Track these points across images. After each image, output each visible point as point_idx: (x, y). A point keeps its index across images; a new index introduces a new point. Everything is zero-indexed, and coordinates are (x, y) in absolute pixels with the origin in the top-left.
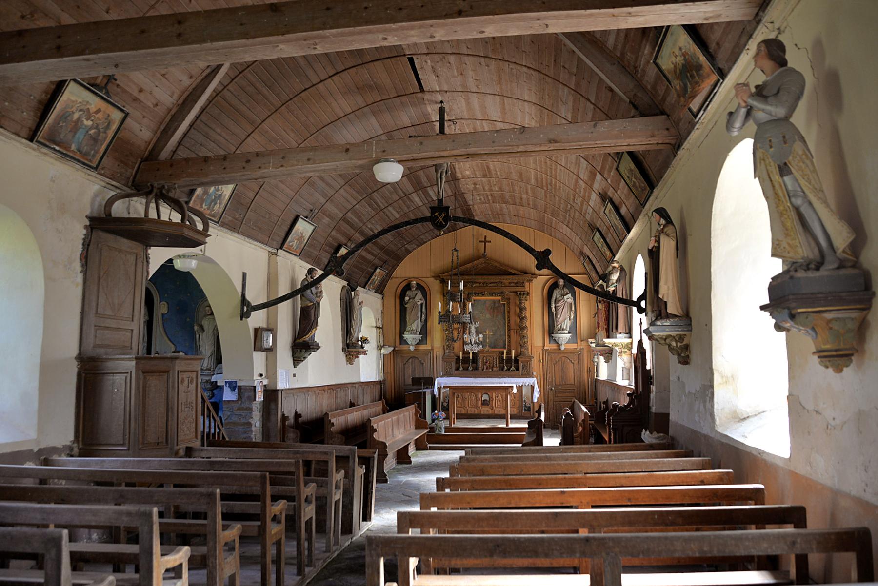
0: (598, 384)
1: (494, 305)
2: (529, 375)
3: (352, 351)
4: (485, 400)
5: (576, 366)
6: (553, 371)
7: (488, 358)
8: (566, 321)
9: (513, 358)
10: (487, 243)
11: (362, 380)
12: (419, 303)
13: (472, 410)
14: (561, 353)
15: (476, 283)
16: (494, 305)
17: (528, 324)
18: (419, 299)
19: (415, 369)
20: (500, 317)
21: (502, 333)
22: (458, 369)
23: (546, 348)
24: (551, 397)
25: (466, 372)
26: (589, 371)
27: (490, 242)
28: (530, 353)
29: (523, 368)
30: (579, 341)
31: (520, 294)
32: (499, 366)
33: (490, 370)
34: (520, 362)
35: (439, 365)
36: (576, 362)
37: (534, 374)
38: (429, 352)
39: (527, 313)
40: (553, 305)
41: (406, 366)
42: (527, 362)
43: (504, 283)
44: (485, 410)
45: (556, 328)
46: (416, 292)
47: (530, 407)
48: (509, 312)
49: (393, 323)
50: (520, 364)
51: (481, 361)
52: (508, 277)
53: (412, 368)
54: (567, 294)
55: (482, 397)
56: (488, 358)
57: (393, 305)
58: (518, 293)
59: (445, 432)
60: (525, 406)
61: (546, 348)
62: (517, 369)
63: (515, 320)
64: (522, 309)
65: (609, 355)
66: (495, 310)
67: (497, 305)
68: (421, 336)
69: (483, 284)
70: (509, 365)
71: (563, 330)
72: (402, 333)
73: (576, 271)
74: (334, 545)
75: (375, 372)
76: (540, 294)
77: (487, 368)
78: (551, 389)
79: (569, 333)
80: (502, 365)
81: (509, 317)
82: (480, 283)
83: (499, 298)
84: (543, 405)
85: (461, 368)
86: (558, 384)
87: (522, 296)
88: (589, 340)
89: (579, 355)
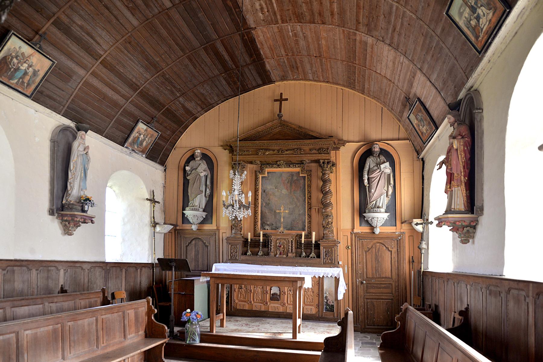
0: (428, 281)
1: (292, 178)
2: (333, 264)
3: (66, 215)
4: (274, 294)
5: (394, 255)
6: (365, 261)
7: (282, 241)
8: (382, 197)
9: (313, 242)
10: (283, 102)
11: (109, 259)
12: (202, 174)
13: (257, 306)
14: (375, 238)
15: (269, 150)
16: (292, 178)
17: (333, 200)
18: (202, 169)
19: (198, 252)
20: (299, 193)
21: (301, 212)
22: (245, 253)
23: (355, 231)
24: (361, 292)
25: (255, 258)
26: (412, 261)
27: (287, 100)
28: (335, 238)
29: (326, 255)
30: (398, 223)
31: (323, 163)
33: (285, 256)
34: (321, 248)
35: (224, 248)
36: (394, 250)
37: (340, 263)
38: (215, 233)
39: (332, 187)
40: (366, 177)
41: (189, 248)
42: (331, 247)
43: (304, 150)
44: (274, 306)
45: (370, 206)
46: (200, 162)
47: (333, 306)
48: (310, 186)
49: (175, 196)
50: (322, 250)
51: (272, 244)
52: (308, 141)
53: (195, 251)
54: (384, 162)
55: (271, 289)
56: (282, 241)
57: (176, 178)
58: (322, 161)
59: (201, 342)
60: (327, 304)
61: (355, 231)
62: (318, 256)
63: (316, 195)
64: (325, 182)
65: (471, 230)
66: (293, 184)
67: (295, 178)
68: (205, 213)
69: (278, 151)
70: (309, 250)
71: (378, 208)
72: (184, 209)
73: (396, 136)
75: (147, 253)
76: (349, 164)
77: (280, 254)
78: (362, 283)
79: (386, 212)
80: (299, 250)
81: (310, 192)
83: (298, 169)
84: (351, 312)
85: (249, 253)
86: (371, 277)
87: (325, 166)
88: (414, 220)
89: (398, 241)
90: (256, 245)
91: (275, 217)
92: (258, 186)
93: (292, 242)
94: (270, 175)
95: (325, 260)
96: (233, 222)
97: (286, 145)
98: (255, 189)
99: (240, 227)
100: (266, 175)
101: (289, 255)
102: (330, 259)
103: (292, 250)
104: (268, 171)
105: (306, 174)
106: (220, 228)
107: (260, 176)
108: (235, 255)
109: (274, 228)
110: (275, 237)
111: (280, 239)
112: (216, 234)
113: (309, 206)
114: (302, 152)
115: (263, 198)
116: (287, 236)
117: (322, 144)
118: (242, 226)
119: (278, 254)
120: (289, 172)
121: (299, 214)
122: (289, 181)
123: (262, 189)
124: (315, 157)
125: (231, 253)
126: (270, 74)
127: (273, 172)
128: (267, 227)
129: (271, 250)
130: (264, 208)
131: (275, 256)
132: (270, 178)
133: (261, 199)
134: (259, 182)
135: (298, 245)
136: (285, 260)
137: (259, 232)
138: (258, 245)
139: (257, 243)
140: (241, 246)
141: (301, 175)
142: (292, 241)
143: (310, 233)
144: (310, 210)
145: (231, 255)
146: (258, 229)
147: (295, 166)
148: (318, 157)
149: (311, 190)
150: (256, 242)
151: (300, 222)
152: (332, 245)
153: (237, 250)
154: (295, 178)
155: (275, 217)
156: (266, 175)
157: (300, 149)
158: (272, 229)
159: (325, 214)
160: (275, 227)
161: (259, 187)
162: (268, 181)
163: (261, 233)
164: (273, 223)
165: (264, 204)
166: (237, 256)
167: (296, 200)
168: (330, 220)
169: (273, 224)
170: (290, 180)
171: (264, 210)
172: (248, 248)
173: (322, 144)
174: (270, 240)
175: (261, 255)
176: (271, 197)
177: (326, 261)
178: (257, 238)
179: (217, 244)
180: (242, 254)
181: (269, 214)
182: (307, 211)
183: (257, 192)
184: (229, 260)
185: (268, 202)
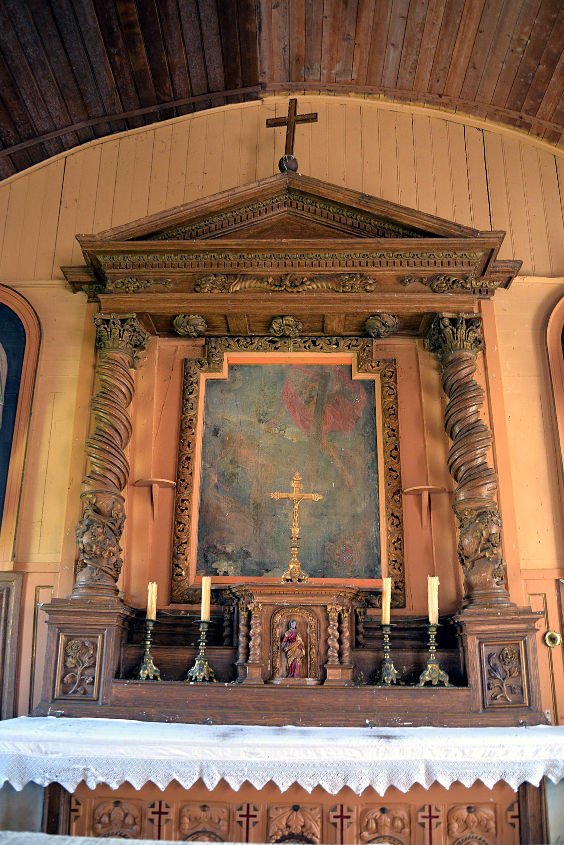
1: (325, 386)
7: (299, 617)
15: (244, 277)
21: (362, 507)
32: (356, 665)
34: (472, 643)
51: (256, 630)
56: (299, 617)
66: (328, 409)
67: (335, 386)
74: (440, 823)
80: (368, 655)
82: (260, 278)
90: (176, 634)
91: (258, 524)
92: (192, 413)
93: (340, 621)
94: (238, 374)
95: (489, 694)
96: (85, 540)
97: (309, 262)
98: (181, 421)
99: (114, 560)
100: (224, 374)
101: (329, 677)
102: (511, 690)
103: (340, 654)
104: (232, 362)
105: (378, 371)
106: (31, 568)
107: (203, 378)
108: (82, 680)
109: (255, 567)
110: (266, 600)
111: (292, 606)
112: (9, 592)
113: (395, 483)
114: (370, 284)
115: (209, 458)
116: (321, 595)
117: (445, 261)
118: (122, 556)
119: (282, 671)
120: (311, 366)
121: (354, 516)
122: (311, 397)
123: (205, 423)
124: (420, 302)
125: (66, 670)
126: (260, 30)
127: (249, 366)
128: (223, 566)
129: (247, 655)
130: (211, 493)
131: (266, 682)
132: (238, 384)
133: (203, 458)
134: (197, 397)
135: (357, 633)
136: (315, 699)
137: (192, 580)
138: (185, 635)
139: (180, 630)
140: (112, 644)
141: (357, 376)
142: (339, 615)
143: (400, 584)
144: (396, 497)
145: (67, 679)
146: (187, 574)
147: (337, 344)
148: (430, 305)
149: (398, 427)
150: (175, 625)
151: (359, 545)
152: (518, 631)
153: (93, 656)
154: (335, 386)
155: (258, 524)
156: (224, 374)
157: (362, 275)
158: (244, 572)
159: (473, 505)
160: (258, 564)
161: (195, 416)
162: (231, 395)
163: (206, 584)
164: (250, 550)
165: (215, 478)
166: (92, 683)
167: (339, 464)
168: (494, 530)
169: (247, 554)
170: (314, 393)
171: (214, 501)
172: (144, 647)
173: (445, 261)
174: (243, 615)
175: (204, 679)
176: (243, 451)
177: (494, 698)
178: (182, 607)
179: (10, 632)
180: (117, 676)
181: (233, 515)
182: (388, 501)
183: (189, 433)
184: (54, 700)
185: (231, 469)
